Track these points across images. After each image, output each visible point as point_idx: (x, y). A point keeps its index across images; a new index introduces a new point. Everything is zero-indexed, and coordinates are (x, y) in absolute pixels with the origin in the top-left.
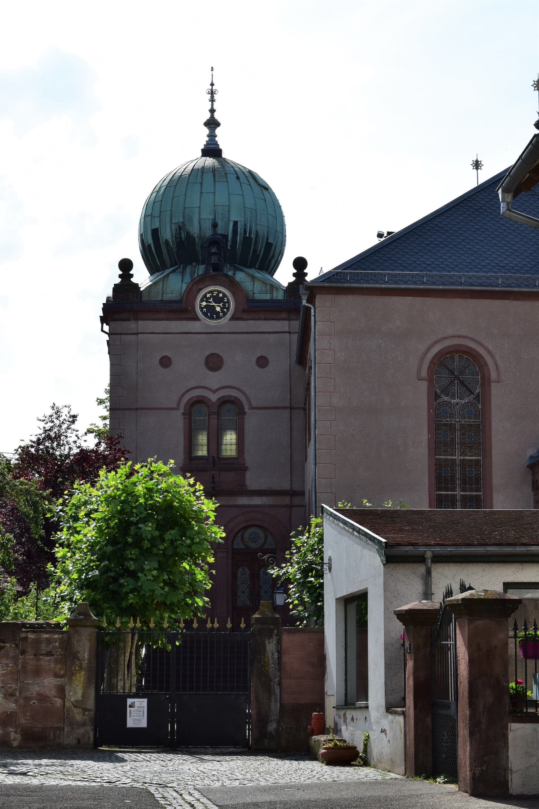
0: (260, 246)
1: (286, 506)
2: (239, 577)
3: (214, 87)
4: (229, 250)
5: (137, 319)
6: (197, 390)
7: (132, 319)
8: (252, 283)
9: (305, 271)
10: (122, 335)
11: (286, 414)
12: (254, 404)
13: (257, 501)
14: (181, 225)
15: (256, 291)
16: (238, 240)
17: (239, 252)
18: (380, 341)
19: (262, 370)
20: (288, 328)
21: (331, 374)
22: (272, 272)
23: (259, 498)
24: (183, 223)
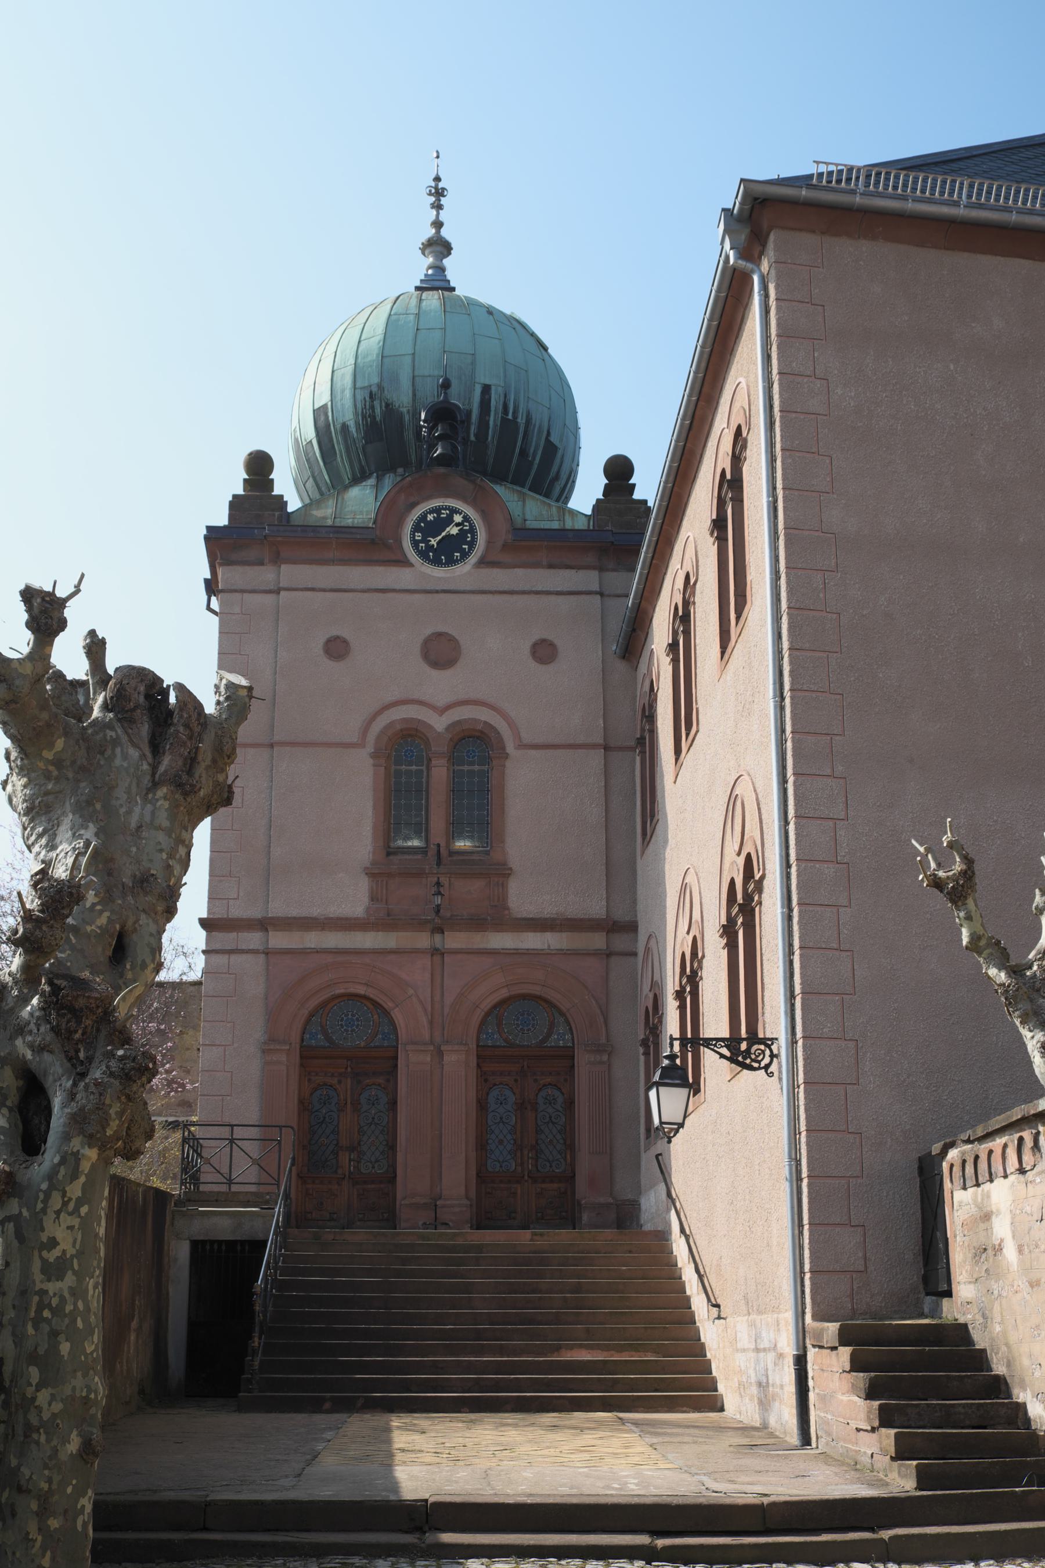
0: (534, 444)
1: (595, 953)
2: (490, 1110)
3: (441, 185)
4: (472, 442)
5: (277, 560)
6: (404, 707)
7: (266, 561)
8: (520, 503)
9: (631, 481)
10: (246, 595)
11: (596, 759)
12: (527, 737)
13: (532, 941)
14: (374, 389)
15: (528, 517)
16: (491, 423)
17: (491, 451)
18: (952, 367)
19: (542, 668)
20: (598, 586)
21: (821, 444)
23: (539, 934)
24: (380, 387)
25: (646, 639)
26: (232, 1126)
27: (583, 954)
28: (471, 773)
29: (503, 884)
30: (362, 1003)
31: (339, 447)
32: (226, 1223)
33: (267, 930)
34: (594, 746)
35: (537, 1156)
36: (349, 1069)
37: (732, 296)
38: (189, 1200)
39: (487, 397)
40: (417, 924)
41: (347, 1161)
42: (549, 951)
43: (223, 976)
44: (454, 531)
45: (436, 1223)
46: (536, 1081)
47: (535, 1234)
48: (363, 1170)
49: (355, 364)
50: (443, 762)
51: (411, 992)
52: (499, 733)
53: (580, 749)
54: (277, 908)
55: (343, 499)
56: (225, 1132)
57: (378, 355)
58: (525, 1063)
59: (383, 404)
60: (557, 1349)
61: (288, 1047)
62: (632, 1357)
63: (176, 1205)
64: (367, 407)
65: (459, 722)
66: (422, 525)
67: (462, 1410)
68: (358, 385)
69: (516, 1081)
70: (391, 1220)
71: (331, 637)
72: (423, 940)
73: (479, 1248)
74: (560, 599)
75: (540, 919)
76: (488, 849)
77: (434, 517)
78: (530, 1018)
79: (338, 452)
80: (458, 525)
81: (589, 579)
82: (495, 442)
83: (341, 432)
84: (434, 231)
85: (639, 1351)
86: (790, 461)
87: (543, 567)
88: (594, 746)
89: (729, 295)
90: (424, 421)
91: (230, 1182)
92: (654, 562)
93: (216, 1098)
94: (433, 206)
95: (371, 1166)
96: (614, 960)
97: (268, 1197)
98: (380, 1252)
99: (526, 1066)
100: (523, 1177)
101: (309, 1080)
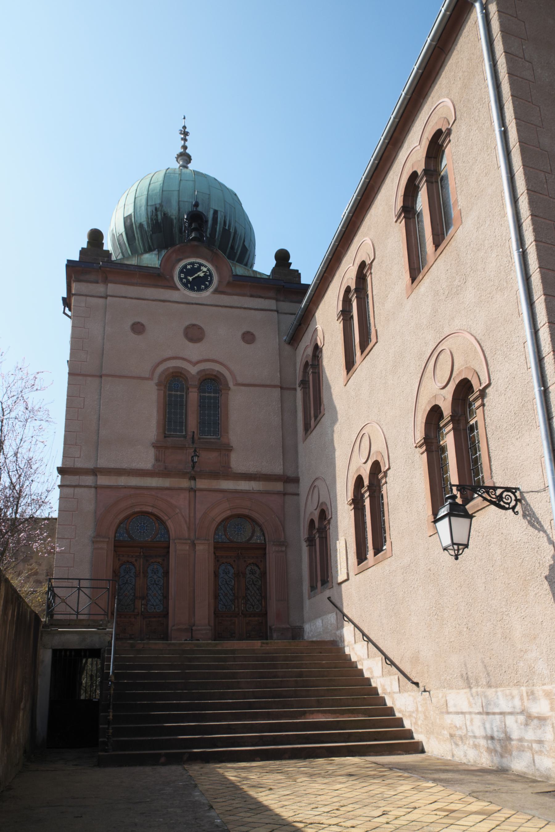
1: (278, 493)
3: (186, 130)
5: (106, 281)
9: (290, 261)
10: (88, 298)
11: (276, 393)
12: (240, 380)
13: (244, 485)
14: (158, 206)
16: (218, 229)
19: (248, 346)
22: (252, 266)
23: (247, 482)
24: (161, 205)
25: (307, 329)
26: (80, 580)
28: (210, 398)
29: (228, 455)
30: (149, 517)
31: (137, 235)
32: (76, 638)
33: (96, 475)
34: (275, 386)
36: (142, 554)
37: (438, 47)
38: (52, 625)
39: (216, 216)
40: (181, 474)
41: (140, 605)
42: (253, 491)
43: (70, 499)
44: (202, 274)
45: (192, 639)
46: (245, 561)
47: (263, 643)
48: (149, 611)
49: (148, 194)
50: (196, 390)
51: (178, 511)
54: (103, 463)
55: (140, 258)
56: (76, 583)
57: (160, 190)
58: (239, 552)
59: (163, 214)
60: (303, 714)
61: (107, 540)
62: (350, 717)
63: (43, 627)
64: (154, 215)
65: (204, 370)
66: (185, 270)
67: (256, 759)
68: (149, 204)
69: (234, 561)
70: (165, 637)
71: (135, 322)
72: (185, 483)
73: (233, 651)
74: (257, 312)
75: (248, 474)
76: (219, 437)
79: (136, 238)
81: (271, 304)
82: (219, 239)
83: (139, 228)
84: (182, 150)
85: (354, 714)
86: (517, 103)
87: (248, 296)
88: (275, 386)
89: (437, 45)
90: (186, 219)
91: (78, 613)
92: (325, 275)
93: (65, 568)
94: (182, 139)
95: (153, 608)
96: (287, 497)
97: (101, 622)
98: (173, 655)
99: (240, 554)
100: (239, 614)
101: (119, 559)
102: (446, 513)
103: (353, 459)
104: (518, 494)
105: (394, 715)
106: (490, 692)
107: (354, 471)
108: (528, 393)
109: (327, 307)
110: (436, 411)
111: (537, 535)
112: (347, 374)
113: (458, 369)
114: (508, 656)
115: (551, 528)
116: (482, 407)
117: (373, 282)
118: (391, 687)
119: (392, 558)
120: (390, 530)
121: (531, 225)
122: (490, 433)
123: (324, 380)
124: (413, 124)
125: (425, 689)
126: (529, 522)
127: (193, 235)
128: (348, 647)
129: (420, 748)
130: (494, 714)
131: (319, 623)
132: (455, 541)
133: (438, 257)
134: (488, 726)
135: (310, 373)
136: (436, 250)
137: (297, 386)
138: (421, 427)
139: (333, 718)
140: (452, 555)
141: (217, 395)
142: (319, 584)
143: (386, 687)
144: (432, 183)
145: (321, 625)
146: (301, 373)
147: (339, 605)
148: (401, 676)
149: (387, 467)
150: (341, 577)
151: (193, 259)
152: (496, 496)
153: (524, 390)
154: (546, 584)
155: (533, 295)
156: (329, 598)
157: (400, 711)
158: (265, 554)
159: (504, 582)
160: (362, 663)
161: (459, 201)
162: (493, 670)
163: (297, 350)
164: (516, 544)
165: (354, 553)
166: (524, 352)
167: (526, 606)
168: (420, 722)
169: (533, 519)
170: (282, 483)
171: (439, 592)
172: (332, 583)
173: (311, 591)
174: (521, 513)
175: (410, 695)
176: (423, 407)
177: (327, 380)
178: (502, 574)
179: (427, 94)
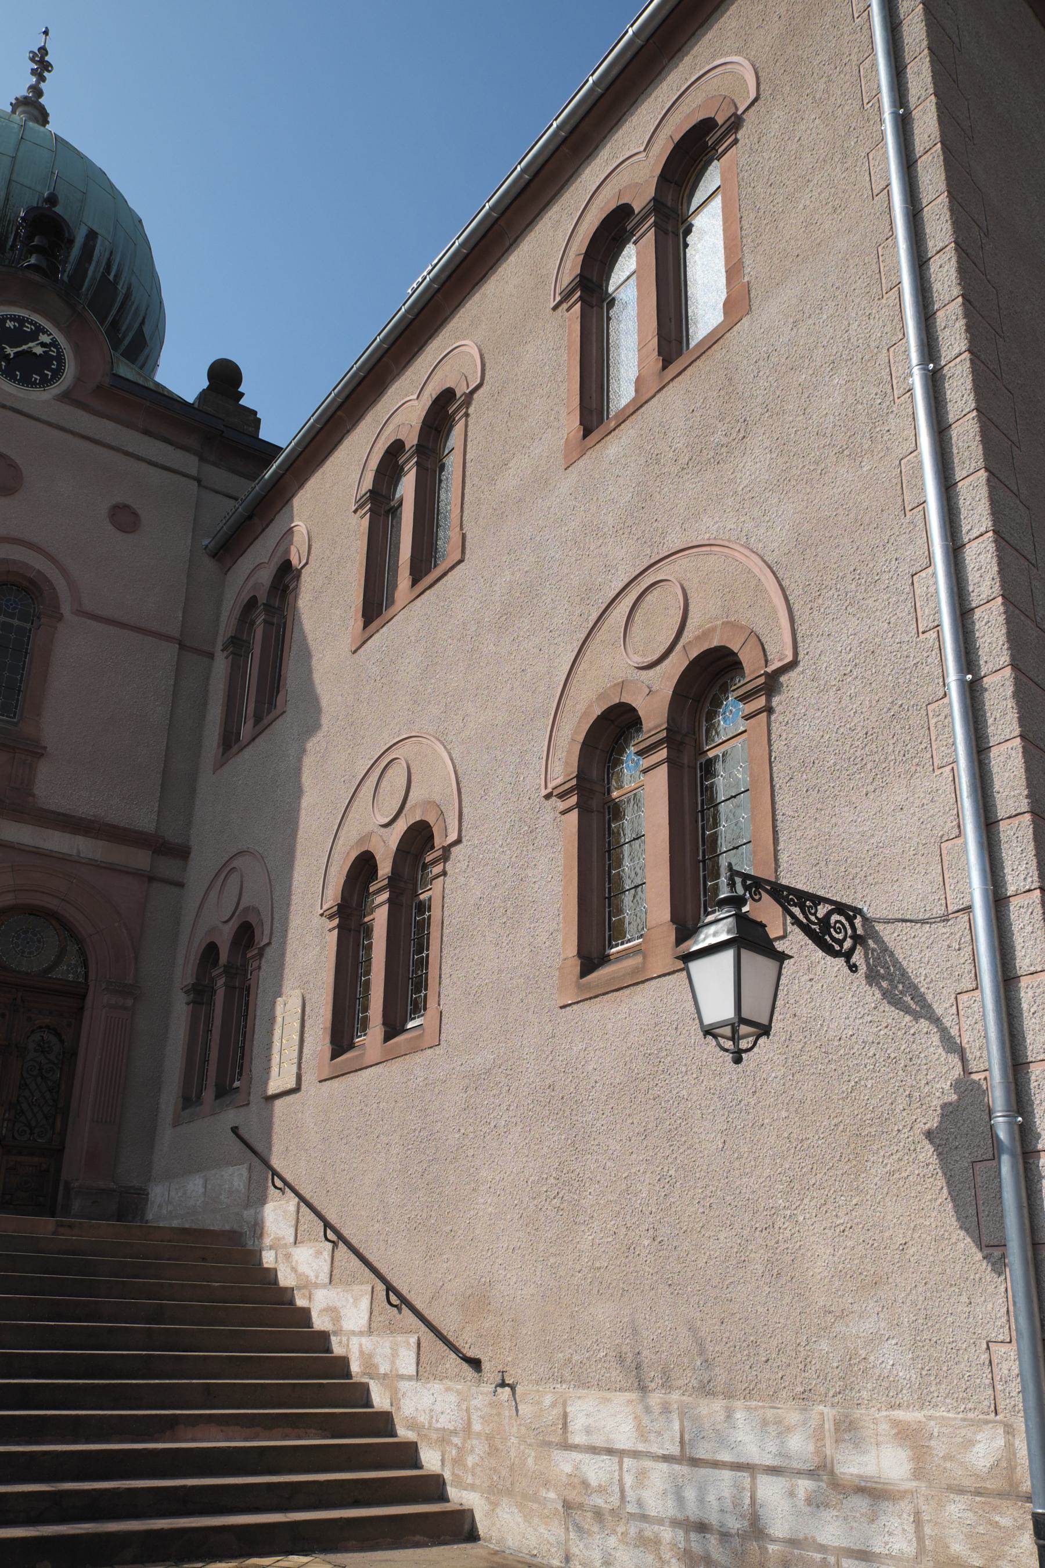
0: (127, 322)
1: (137, 874)
9: (240, 390)
11: (169, 652)
13: (57, 842)
23: (68, 836)
25: (263, 530)
27: (120, 871)
34: (168, 638)
35: (15, 1117)
44: (39, 351)
47: (61, 1225)
52: (54, 589)
53: (150, 636)
60: (168, 1427)
74: (152, 470)
76: (15, 720)
77: (14, 326)
78: (35, 938)
80: (43, 345)
81: (190, 463)
82: (89, 296)
88: (168, 638)
90: (22, 218)
92: (339, 413)
94: (33, 72)
102: (724, 937)
103: (352, 815)
104: (858, 922)
105: (393, 1434)
106: (712, 1409)
107: (352, 842)
108: (912, 688)
109: (328, 485)
110: (613, 721)
111: (910, 1027)
112: (365, 627)
113: (700, 626)
114: (782, 1321)
115: (958, 1014)
116: (765, 714)
117: (469, 434)
118: (393, 1363)
119: (438, 1050)
120: (440, 984)
121: (960, 316)
122: (781, 775)
123: (294, 639)
124: (632, 110)
125: (503, 1380)
126: (885, 994)
127: (33, 260)
128: (273, 1253)
129: (467, 1527)
130: (716, 1465)
131: (195, 1185)
132: (745, 1014)
133: (668, 383)
134: (690, 1494)
135: (259, 621)
136: (664, 368)
137: (219, 646)
138: (569, 752)
139: (246, 1440)
140: (727, 1050)
141: (28, 626)
142: (209, 1094)
143: (377, 1360)
144: (666, 233)
145: (201, 1190)
146: (234, 622)
147: (259, 1148)
148: (428, 1336)
149: (453, 837)
150: (279, 1079)
151: (24, 311)
152: (817, 918)
153: (901, 681)
154: (927, 1152)
155: (953, 469)
156: (235, 1130)
157: (413, 1425)
158: (82, 1009)
159: (786, 1135)
160: (310, 1295)
161: (746, 265)
162: (727, 1353)
163: (230, 574)
164: (836, 1043)
165: (325, 1029)
166: (911, 595)
167: (854, 1202)
168: (470, 1460)
169: (900, 987)
170: (150, 852)
171: (573, 1143)
172: (249, 1093)
173: (184, 1108)
174: (863, 969)
175: (448, 1389)
176: (581, 707)
177: (304, 638)
178: (784, 1114)
179: (660, 73)
